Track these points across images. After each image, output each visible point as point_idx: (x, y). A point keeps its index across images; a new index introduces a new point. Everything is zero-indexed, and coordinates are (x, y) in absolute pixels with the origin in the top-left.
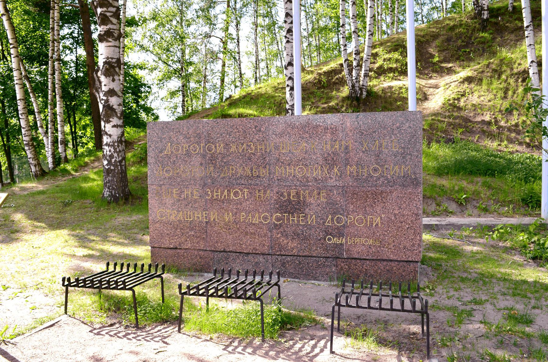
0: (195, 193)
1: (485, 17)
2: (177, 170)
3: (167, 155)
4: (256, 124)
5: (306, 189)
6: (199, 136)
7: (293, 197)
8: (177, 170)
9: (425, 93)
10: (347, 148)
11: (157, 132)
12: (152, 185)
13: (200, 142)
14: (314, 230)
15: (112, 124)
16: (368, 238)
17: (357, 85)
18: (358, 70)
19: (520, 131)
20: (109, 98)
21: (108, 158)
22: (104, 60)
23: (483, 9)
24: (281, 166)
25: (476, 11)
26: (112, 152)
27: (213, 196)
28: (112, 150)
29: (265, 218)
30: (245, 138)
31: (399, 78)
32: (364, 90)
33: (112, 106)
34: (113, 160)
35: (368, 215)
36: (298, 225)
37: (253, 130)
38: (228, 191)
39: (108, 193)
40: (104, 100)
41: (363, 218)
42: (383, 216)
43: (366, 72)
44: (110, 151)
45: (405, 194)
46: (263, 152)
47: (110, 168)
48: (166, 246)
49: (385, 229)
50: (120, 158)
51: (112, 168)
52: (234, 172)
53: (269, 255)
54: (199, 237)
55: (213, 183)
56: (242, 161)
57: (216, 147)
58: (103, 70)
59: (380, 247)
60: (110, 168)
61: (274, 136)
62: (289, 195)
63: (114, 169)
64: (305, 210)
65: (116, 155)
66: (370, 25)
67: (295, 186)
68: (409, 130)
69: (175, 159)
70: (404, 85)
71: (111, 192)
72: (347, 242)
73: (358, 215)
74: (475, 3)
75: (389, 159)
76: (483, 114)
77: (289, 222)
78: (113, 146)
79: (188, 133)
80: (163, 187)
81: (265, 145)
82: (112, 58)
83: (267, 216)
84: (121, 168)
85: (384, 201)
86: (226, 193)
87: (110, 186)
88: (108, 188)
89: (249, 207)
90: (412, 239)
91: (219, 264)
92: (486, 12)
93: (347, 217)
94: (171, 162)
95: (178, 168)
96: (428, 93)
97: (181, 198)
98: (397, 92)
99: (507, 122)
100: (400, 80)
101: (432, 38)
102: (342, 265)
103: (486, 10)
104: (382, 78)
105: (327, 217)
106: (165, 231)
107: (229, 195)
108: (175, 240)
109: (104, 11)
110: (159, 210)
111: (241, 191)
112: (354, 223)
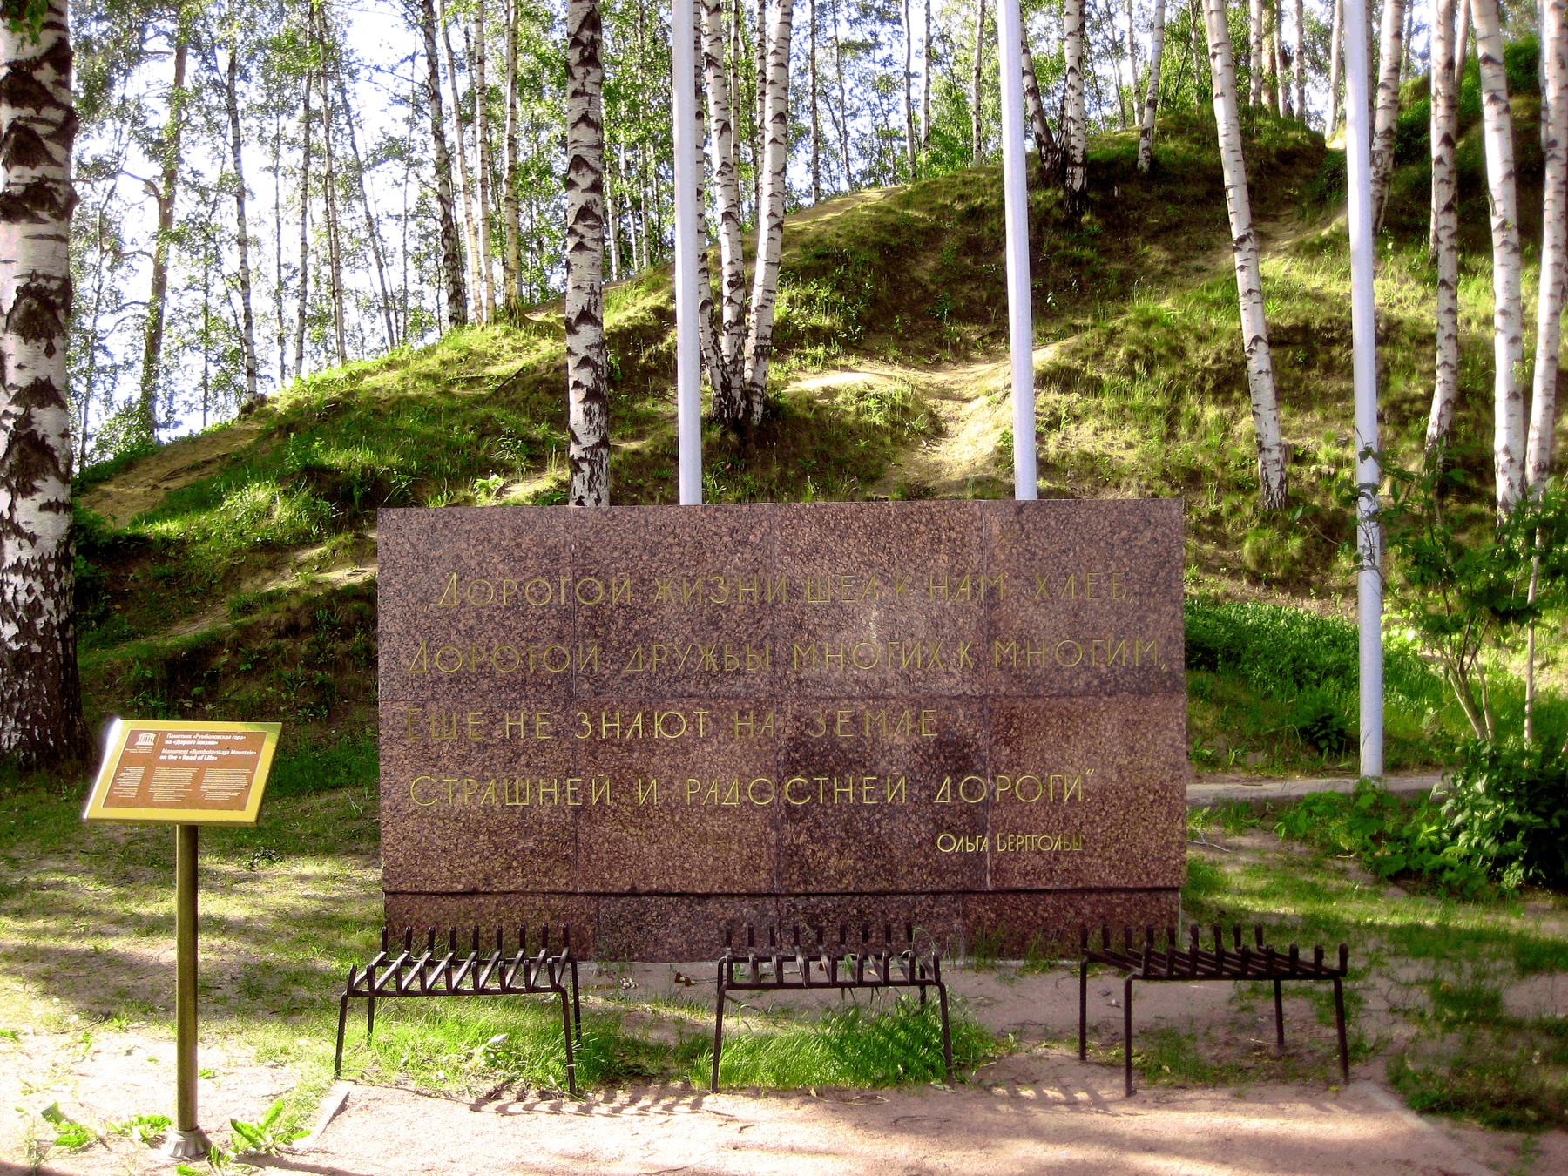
0: (539, 723)
1: (1077, 185)
2: (480, 654)
3: (447, 609)
4: (731, 521)
5: (879, 707)
6: (553, 554)
7: (843, 727)
8: (480, 654)
9: (931, 414)
10: (992, 592)
11: (414, 541)
12: (393, 701)
13: (557, 573)
14: (901, 818)
15: (39, 498)
16: (1049, 833)
17: (736, 382)
18: (739, 335)
19: (1225, 536)
20: (35, 410)
21: (19, 614)
22: (19, 283)
23: (1067, 159)
24: (808, 644)
25: (1047, 165)
26: (38, 593)
27: (598, 733)
28: (38, 587)
29: (761, 791)
30: (699, 563)
31: (841, 361)
32: (757, 399)
33: (44, 437)
34: (40, 623)
35: (1050, 771)
36: (858, 807)
37: (726, 539)
38: (644, 715)
39: (16, 736)
40: (15, 416)
41: (1036, 779)
42: (1089, 772)
43: (763, 343)
44: (30, 591)
45: (1145, 712)
46: (755, 602)
47: (28, 648)
48: (440, 887)
49: (1096, 808)
50: (63, 616)
51: (36, 648)
52: (663, 660)
53: (769, 895)
54: (550, 855)
55: (597, 694)
56: (689, 629)
57: (607, 587)
58: (16, 316)
59: (1081, 854)
60: (28, 648)
61: (787, 559)
62: (831, 722)
63: (43, 655)
64: (876, 764)
65: (49, 604)
66: (772, 195)
67: (850, 698)
68: (1153, 549)
69: (471, 622)
70: (870, 388)
71: (30, 733)
72: (993, 848)
73: (1024, 773)
74: (1044, 139)
75: (1102, 622)
76: (1117, 486)
77: (832, 799)
78: (41, 573)
79: (518, 545)
80: (432, 706)
81: (762, 584)
82: (48, 278)
83: (765, 784)
84: (65, 648)
85: (1093, 733)
86: (638, 722)
87: (26, 713)
88: (19, 718)
89: (711, 762)
90: (1164, 831)
91: (613, 931)
92: (1079, 171)
93: (994, 779)
94: (458, 631)
95: (483, 650)
96: (943, 414)
97: (492, 738)
98: (852, 409)
99: (1188, 508)
100: (845, 368)
101: (922, 238)
102: (981, 910)
103: (1080, 165)
104: (793, 362)
105: (940, 782)
106: (438, 842)
107: (648, 727)
108: (472, 868)
109: (26, 119)
110: (415, 777)
111: (687, 715)
112: (1013, 795)
